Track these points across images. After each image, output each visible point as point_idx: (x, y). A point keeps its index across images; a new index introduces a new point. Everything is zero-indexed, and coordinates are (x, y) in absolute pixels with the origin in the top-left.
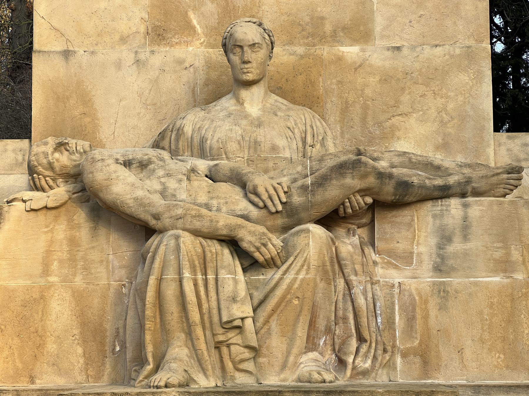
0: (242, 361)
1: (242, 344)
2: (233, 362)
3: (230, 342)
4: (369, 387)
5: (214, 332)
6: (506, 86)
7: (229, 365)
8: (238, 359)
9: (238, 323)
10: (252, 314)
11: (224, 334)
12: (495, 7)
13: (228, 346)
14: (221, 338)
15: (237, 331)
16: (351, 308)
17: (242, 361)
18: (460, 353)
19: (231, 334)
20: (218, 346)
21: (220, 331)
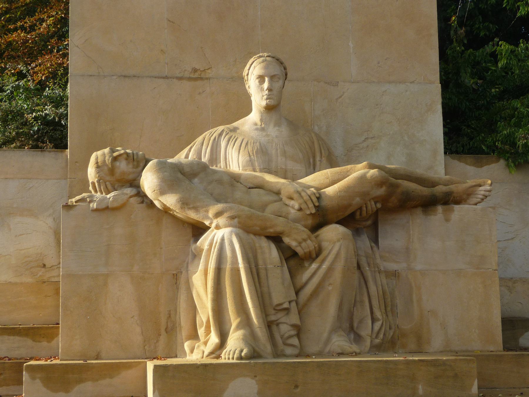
0: (290, 337)
2: (282, 337)
8: (286, 335)
9: (286, 305)
11: (275, 314)
13: (278, 325)
14: (273, 318)
15: (285, 312)
17: (290, 337)
19: (280, 315)
21: (273, 312)
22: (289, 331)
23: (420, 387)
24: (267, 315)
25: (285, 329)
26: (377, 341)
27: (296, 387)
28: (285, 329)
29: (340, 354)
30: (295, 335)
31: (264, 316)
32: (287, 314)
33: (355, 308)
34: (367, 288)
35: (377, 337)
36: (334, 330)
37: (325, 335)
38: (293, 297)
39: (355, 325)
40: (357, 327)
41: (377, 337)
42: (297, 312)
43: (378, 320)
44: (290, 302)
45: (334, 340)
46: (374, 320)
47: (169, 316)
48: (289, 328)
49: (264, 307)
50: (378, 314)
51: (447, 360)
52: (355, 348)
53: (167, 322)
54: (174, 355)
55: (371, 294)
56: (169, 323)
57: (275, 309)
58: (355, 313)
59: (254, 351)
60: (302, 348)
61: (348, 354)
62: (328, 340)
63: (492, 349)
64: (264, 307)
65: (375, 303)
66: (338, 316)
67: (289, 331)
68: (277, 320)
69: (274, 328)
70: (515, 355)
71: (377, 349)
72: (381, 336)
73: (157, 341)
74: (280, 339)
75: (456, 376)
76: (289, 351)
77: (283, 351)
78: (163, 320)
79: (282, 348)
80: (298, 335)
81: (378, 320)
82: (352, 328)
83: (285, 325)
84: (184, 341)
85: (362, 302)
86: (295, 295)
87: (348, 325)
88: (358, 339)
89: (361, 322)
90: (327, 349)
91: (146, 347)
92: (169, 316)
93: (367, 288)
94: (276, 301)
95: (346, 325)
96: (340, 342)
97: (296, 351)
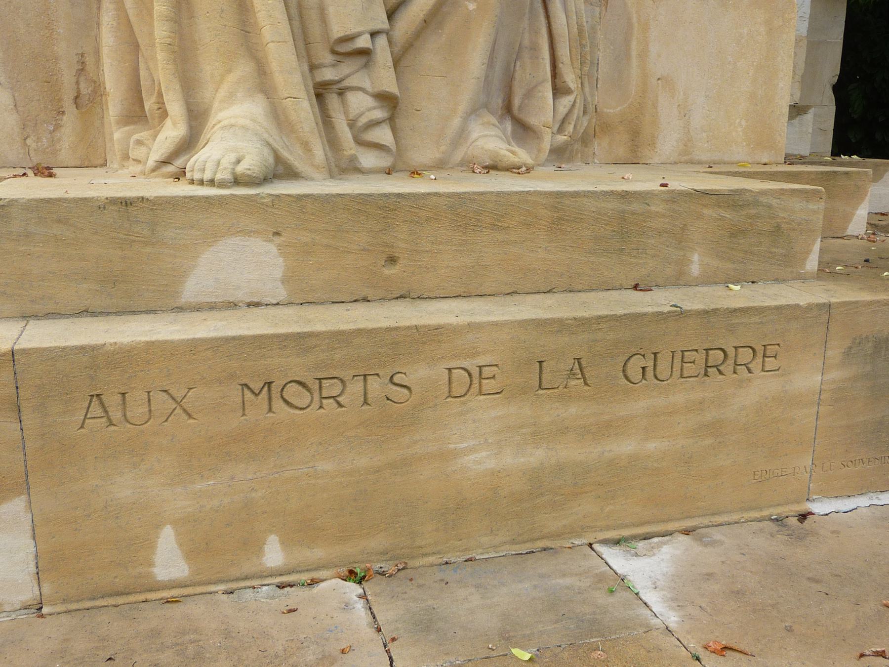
0: (373, 124)
1: (370, 89)
2: (352, 124)
3: (345, 83)
4: (111, 595)
5: (314, 61)
6: (839, 265)
7: (345, 134)
8: (363, 120)
9: (363, 42)
10: (386, 26)
11: (333, 66)
12: (812, 2)
13: (341, 93)
14: (328, 74)
15: (361, 60)
16: (544, 31)
17: (373, 124)
18: (687, 117)
19: (346, 68)
20: (321, 93)
21: (329, 58)
22: (369, 110)
23: (696, 258)
24: (313, 68)
25: (361, 104)
26: (562, 138)
27: (392, 260)
28: (361, 104)
29: (492, 168)
30: (384, 121)
31: (306, 67)
32: (366, 66)
33: (518, 64)
34: (548, 17)
35: (560, 130)
36: (474, 111)
37: (456, 122)
38: (381, 22)
39: (516, 102)
40: (520, 108)
41: (560, 130)
42: (390, 63)
43: (568, 91)
44: (374, 34)
45: (474, 135)
46: (559, 90)
47: (82, 71)
48: (370, 102)
49: (307, 44)
50: (570, 77)
51: (764, 193)
52: (523, 156)
53: (77, 83)
54: (100, 161)
55: (555, 32)
56: (82, 85)
57: (334, 52)
58: (518, 75)
59: (278, 159)
60: (399, 152)
61: (507, 170)
62: (462, 135)
63: (765, 160)
64: (307, 44)
65: (564, 52)
66: (487, 77)
67: (369, 110)
68: (339, 82)
69: (333, 101)
70: (822, 173)
71: (560, 155)
72: (570, 128)
73: (57, 127)
74: (347, 129)
75: (777, 231)
76: (368, 159)
77: (353, 159)
78: (67, 78)
79: (353, 152)
80: (391, 120)
81: (568, 91)
82: (508, 109)
83: (360, 95)
84: (114, 128)
85: (534, 48)
86: (384, 17)
87: (500, 101)
88: (523, 130)
89: (529, 94)
90: (458, 156)
91: (29, 141)
92: (82, 71)
93: (548, 17)
94: (337, 31)
95: (498, 101)
96: (490, 139)
97: (385, 161)
